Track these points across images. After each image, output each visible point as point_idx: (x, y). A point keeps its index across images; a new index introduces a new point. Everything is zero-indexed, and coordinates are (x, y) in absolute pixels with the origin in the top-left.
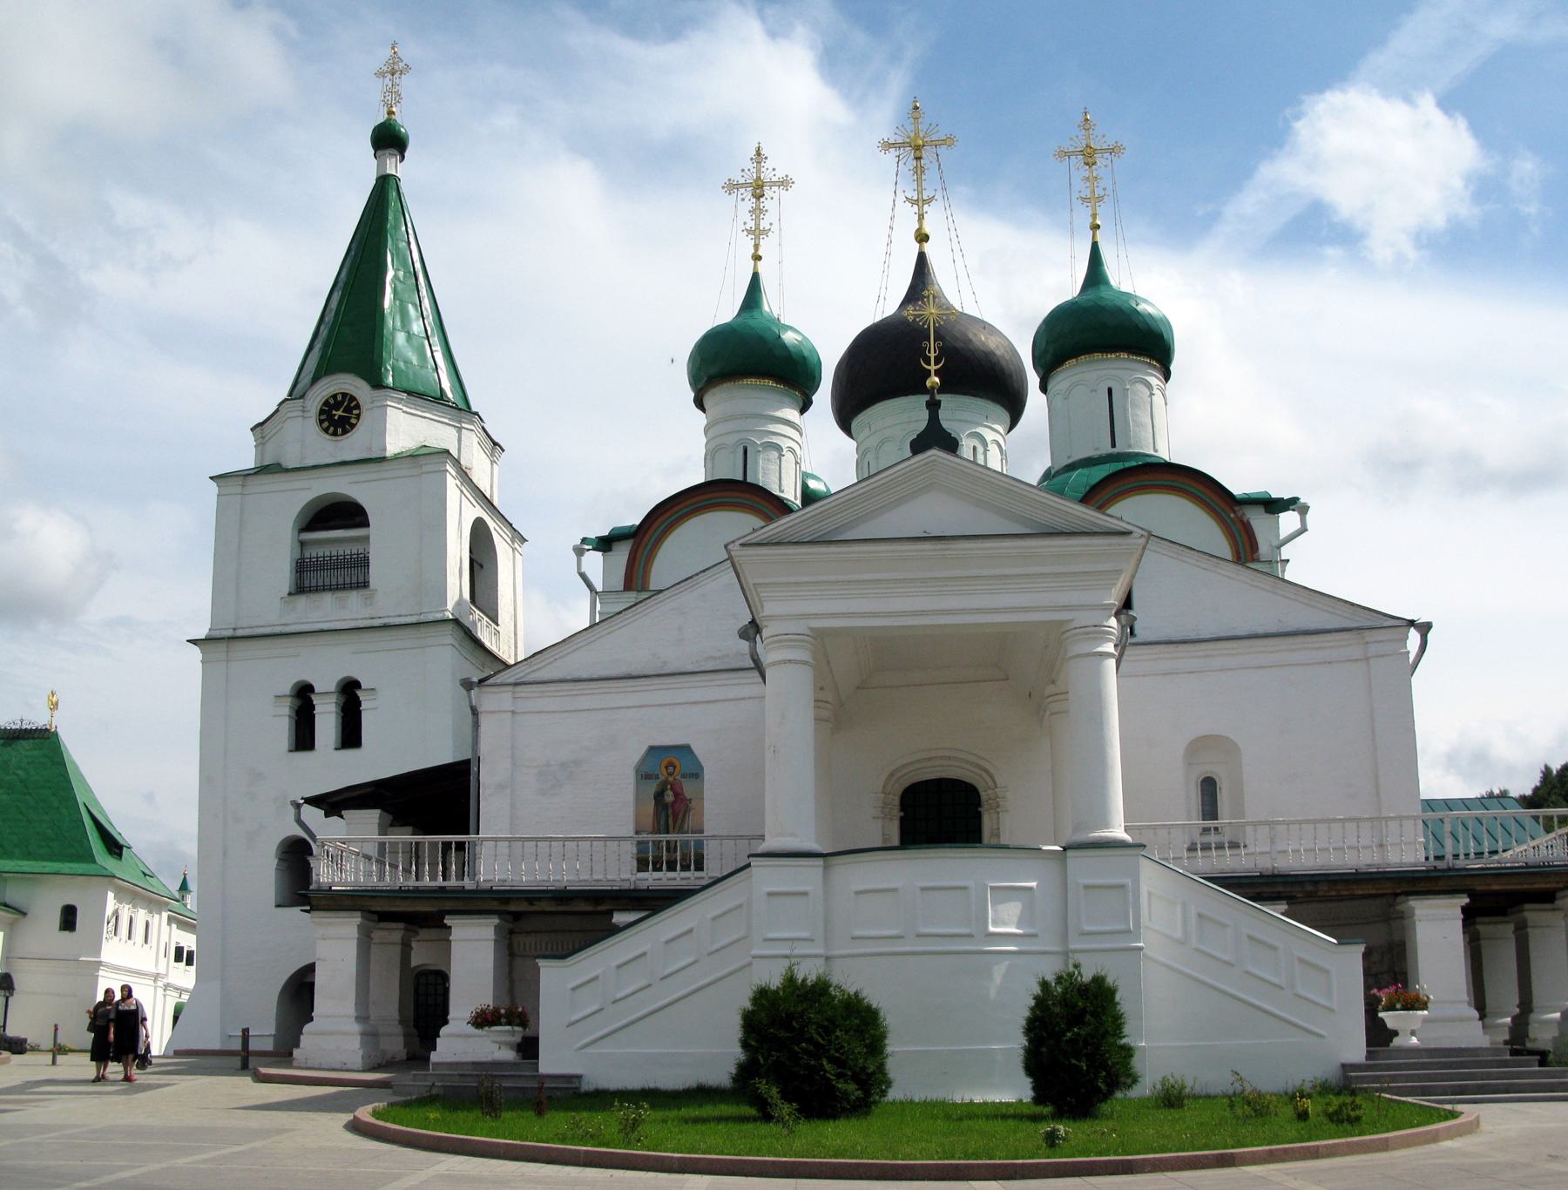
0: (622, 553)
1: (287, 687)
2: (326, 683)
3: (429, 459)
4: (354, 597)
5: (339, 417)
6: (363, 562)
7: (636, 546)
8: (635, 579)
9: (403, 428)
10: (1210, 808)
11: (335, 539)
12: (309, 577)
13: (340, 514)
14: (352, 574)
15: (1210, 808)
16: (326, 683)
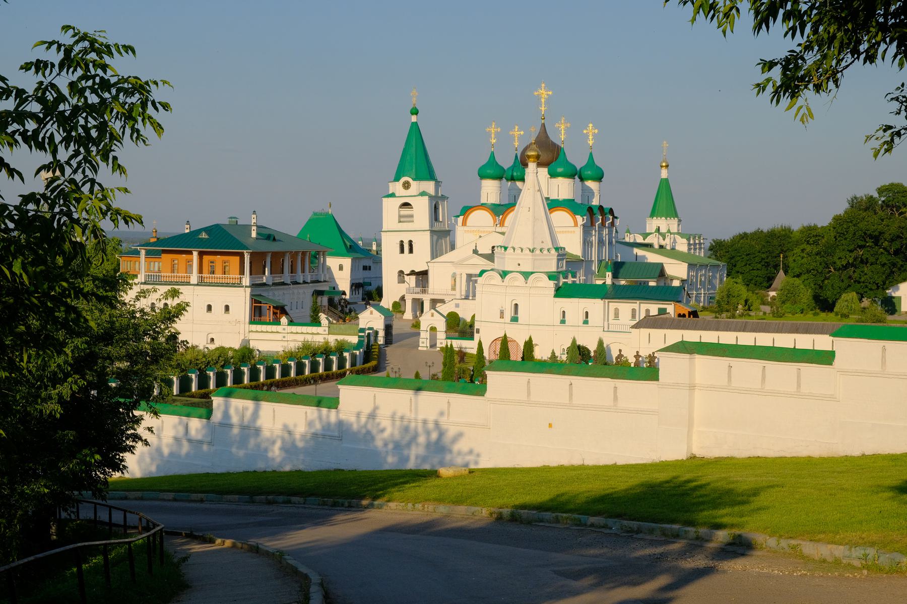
1: (398, 242)
5: (406, 186)
6: (412, 216)
11: (405, 211)
12: (401, 219)
13: (406, 205)
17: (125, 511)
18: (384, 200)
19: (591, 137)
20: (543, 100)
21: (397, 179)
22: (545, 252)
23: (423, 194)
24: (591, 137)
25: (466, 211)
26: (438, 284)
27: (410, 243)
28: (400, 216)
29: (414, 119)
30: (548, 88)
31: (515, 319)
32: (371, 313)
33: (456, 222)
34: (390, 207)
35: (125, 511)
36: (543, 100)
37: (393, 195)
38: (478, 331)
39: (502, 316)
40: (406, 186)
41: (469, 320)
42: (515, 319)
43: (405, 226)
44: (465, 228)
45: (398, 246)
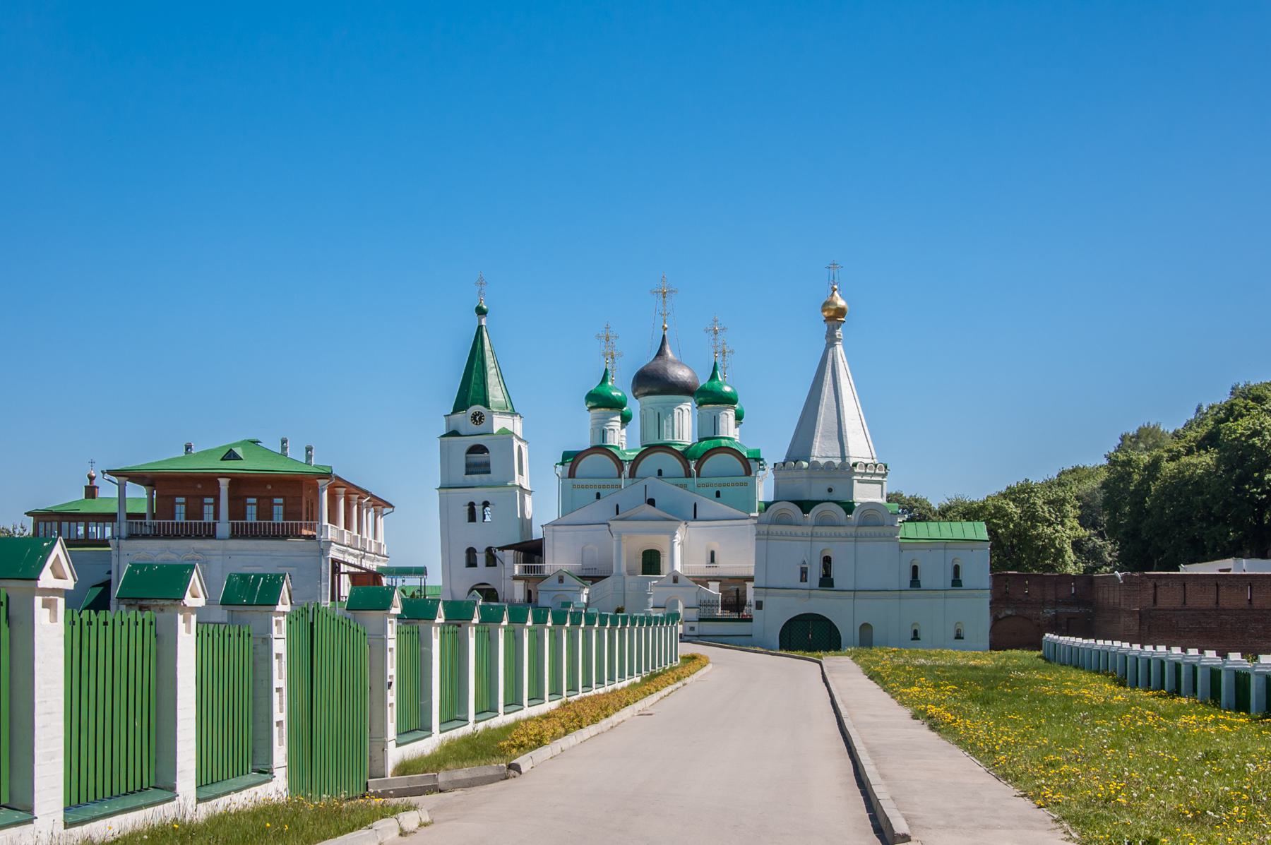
0: (568, 465)
4: (484, 476)
6: (487, 464)
7: (572, 459)
8: (572, 474)
10: (712, 561)
11: (478, 458)
12: (471, 469)
13: (478, 449)
14: (484, 468)
15: (712, 561)
28: (468, 466)
31: (826, 581)
42: (826, 581)
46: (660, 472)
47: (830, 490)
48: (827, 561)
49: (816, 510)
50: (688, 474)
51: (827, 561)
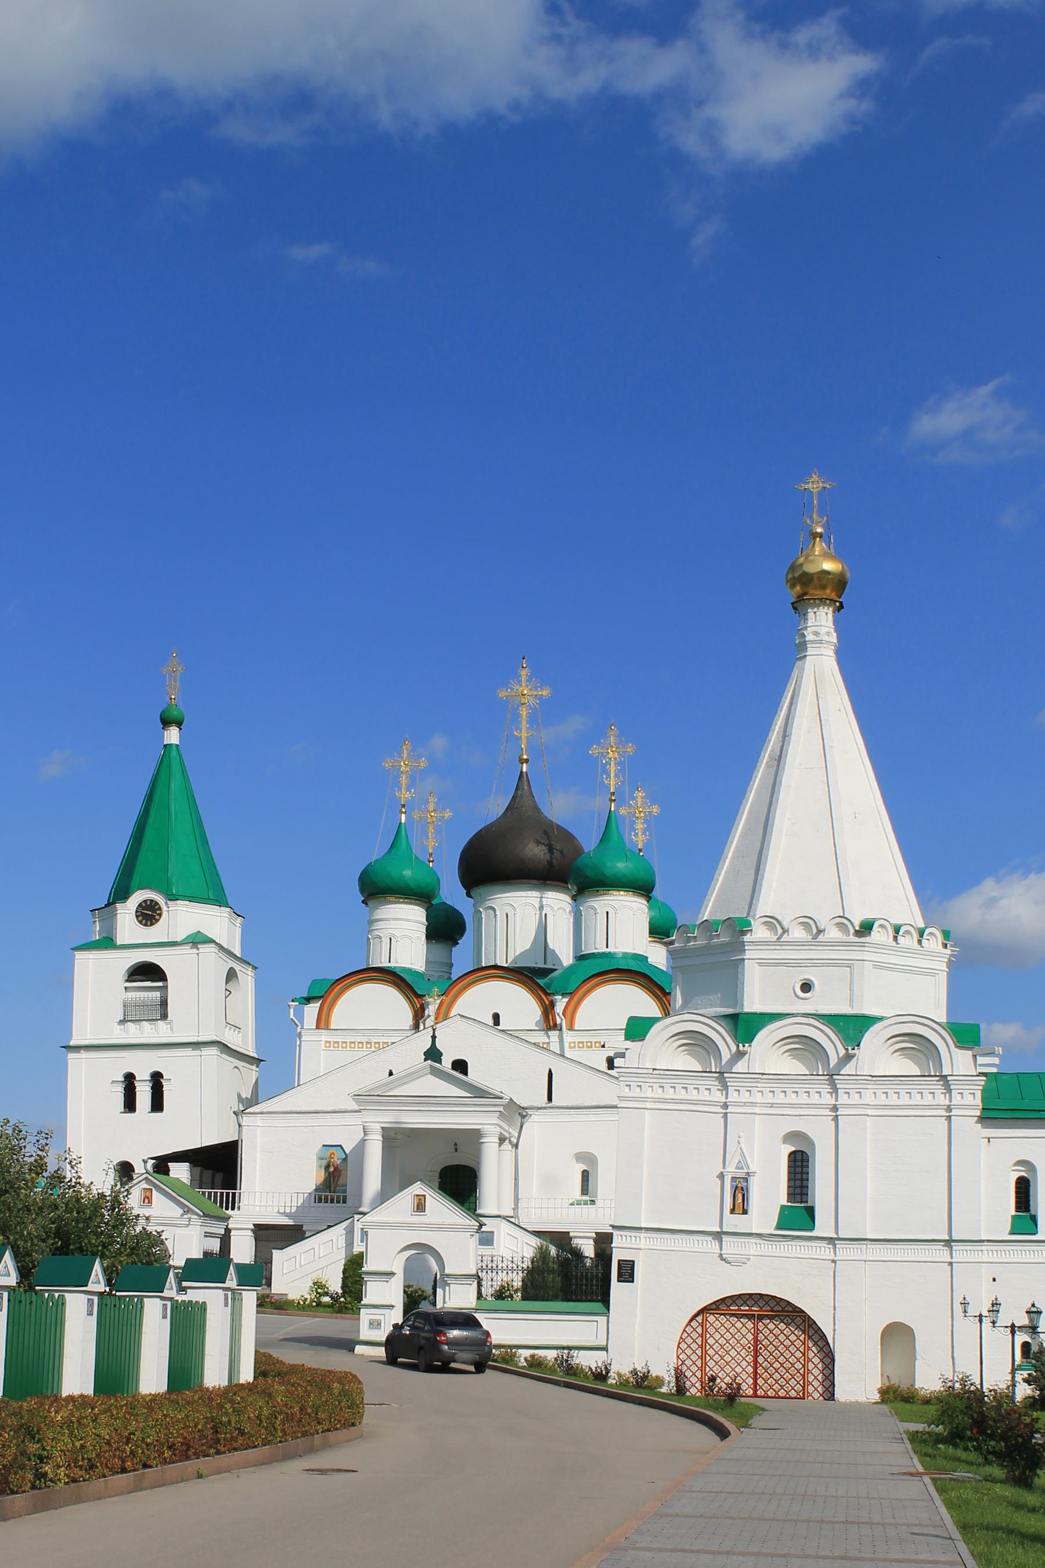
2: (143, 1076)
3: (197, 940)
5: (148, 914)
9: (182, 917)
11: (147, 993)
16: (143, 1076)
17: (562, 1055)
18: (79, 955)
19: (639, 826)
20: (524, 712)
21: (121, 893)
22: (908, 941)
23: (197, 940)
24: (639, 826)
25: (324, 994)
26: (273, 1185)
27: (157, 1079)
29: (173, 736)
30: (539, 676)
31: (799, 1212)
32: (420, 1206)
33: (300, 1016)
34: (98, 983)
35: (562, 1055)
36: (524, 712)
37: (108, 942)
38: (627, 1272)
39: (740, 1207)
40: (148, 914)
41: (535, 1241)
42: (799, 1212)
43: (142, 1066)
44: (324, 1036)
45: (120, 1089)
46: (496, 1018)
47: (806, 987)
48: (800, 1166)
49: (766, 1037)
50: (549, 1023)
51: (800, 1166)
